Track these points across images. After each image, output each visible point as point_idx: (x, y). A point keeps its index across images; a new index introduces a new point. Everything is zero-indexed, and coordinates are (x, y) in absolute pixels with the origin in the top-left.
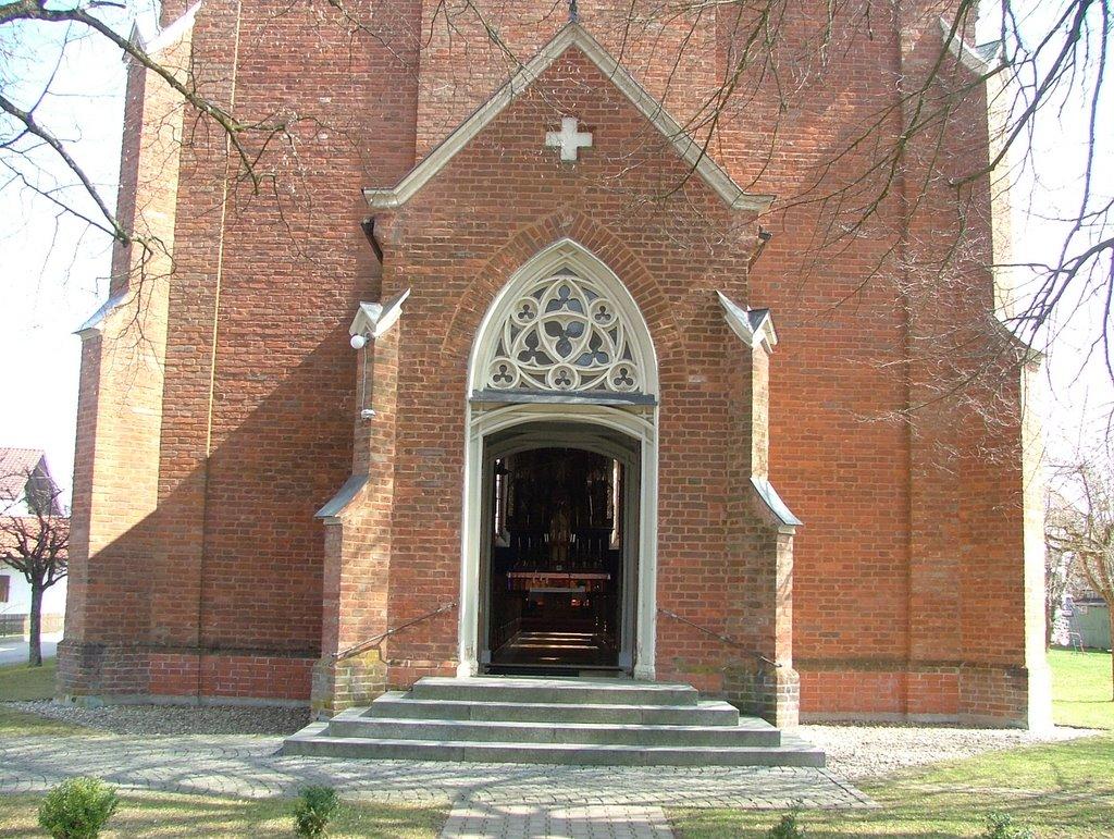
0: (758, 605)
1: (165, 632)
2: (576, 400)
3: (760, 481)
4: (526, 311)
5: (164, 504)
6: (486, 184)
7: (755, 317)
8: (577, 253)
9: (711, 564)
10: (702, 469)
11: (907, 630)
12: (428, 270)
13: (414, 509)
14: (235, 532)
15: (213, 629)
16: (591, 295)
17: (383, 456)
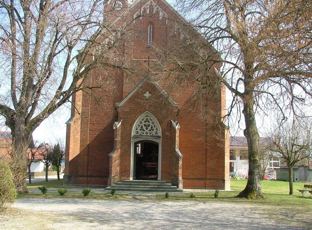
0: (176, 169)
1: (81, 174)
2: (149, 137)
3: (177, 150)
4: (141, 123)
5: (81, 152)
7: (177, 124)
9: (169, 162)
11: (206, 173)
12: (125, 117)
15: (89, 173)
16: (151, 120)
17: (118, 146)
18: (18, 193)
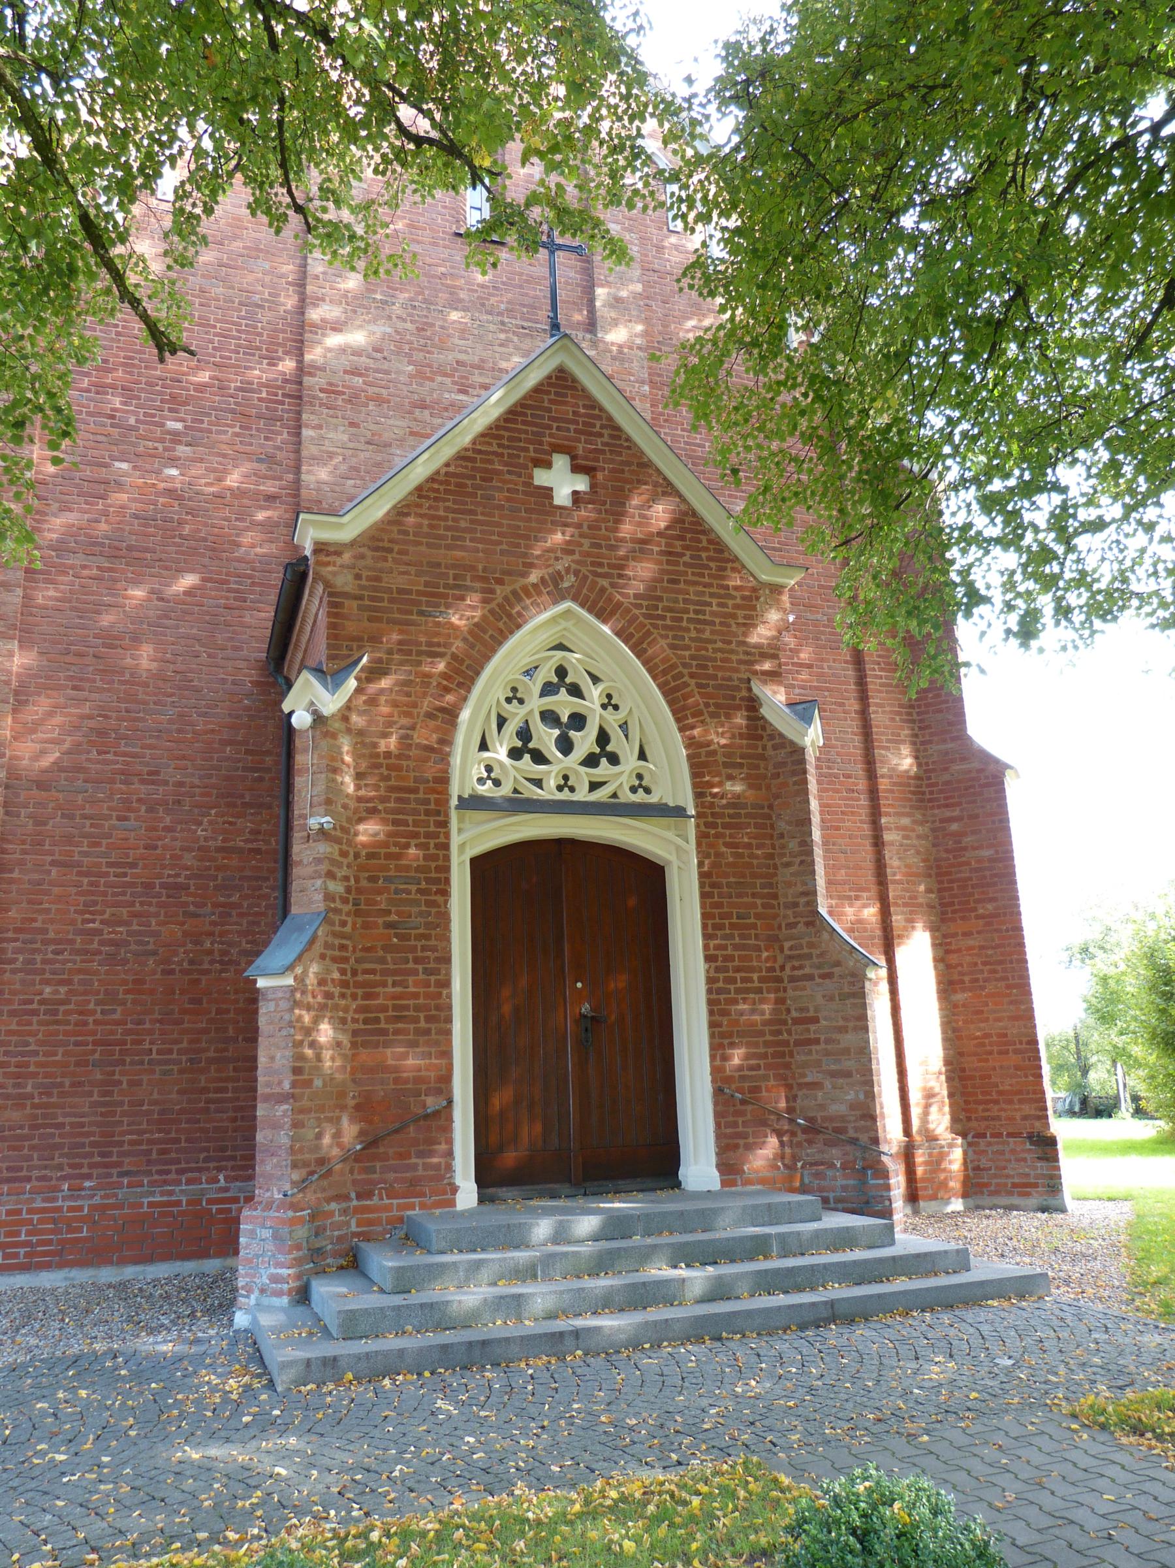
4: (514, 697)
6: (463, 524)
8: (580, 620)
10: (750, 900)
13: (383, 961)
14: (34, 1013)
18: (298, 1262)
